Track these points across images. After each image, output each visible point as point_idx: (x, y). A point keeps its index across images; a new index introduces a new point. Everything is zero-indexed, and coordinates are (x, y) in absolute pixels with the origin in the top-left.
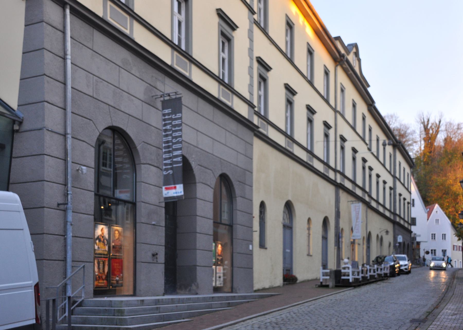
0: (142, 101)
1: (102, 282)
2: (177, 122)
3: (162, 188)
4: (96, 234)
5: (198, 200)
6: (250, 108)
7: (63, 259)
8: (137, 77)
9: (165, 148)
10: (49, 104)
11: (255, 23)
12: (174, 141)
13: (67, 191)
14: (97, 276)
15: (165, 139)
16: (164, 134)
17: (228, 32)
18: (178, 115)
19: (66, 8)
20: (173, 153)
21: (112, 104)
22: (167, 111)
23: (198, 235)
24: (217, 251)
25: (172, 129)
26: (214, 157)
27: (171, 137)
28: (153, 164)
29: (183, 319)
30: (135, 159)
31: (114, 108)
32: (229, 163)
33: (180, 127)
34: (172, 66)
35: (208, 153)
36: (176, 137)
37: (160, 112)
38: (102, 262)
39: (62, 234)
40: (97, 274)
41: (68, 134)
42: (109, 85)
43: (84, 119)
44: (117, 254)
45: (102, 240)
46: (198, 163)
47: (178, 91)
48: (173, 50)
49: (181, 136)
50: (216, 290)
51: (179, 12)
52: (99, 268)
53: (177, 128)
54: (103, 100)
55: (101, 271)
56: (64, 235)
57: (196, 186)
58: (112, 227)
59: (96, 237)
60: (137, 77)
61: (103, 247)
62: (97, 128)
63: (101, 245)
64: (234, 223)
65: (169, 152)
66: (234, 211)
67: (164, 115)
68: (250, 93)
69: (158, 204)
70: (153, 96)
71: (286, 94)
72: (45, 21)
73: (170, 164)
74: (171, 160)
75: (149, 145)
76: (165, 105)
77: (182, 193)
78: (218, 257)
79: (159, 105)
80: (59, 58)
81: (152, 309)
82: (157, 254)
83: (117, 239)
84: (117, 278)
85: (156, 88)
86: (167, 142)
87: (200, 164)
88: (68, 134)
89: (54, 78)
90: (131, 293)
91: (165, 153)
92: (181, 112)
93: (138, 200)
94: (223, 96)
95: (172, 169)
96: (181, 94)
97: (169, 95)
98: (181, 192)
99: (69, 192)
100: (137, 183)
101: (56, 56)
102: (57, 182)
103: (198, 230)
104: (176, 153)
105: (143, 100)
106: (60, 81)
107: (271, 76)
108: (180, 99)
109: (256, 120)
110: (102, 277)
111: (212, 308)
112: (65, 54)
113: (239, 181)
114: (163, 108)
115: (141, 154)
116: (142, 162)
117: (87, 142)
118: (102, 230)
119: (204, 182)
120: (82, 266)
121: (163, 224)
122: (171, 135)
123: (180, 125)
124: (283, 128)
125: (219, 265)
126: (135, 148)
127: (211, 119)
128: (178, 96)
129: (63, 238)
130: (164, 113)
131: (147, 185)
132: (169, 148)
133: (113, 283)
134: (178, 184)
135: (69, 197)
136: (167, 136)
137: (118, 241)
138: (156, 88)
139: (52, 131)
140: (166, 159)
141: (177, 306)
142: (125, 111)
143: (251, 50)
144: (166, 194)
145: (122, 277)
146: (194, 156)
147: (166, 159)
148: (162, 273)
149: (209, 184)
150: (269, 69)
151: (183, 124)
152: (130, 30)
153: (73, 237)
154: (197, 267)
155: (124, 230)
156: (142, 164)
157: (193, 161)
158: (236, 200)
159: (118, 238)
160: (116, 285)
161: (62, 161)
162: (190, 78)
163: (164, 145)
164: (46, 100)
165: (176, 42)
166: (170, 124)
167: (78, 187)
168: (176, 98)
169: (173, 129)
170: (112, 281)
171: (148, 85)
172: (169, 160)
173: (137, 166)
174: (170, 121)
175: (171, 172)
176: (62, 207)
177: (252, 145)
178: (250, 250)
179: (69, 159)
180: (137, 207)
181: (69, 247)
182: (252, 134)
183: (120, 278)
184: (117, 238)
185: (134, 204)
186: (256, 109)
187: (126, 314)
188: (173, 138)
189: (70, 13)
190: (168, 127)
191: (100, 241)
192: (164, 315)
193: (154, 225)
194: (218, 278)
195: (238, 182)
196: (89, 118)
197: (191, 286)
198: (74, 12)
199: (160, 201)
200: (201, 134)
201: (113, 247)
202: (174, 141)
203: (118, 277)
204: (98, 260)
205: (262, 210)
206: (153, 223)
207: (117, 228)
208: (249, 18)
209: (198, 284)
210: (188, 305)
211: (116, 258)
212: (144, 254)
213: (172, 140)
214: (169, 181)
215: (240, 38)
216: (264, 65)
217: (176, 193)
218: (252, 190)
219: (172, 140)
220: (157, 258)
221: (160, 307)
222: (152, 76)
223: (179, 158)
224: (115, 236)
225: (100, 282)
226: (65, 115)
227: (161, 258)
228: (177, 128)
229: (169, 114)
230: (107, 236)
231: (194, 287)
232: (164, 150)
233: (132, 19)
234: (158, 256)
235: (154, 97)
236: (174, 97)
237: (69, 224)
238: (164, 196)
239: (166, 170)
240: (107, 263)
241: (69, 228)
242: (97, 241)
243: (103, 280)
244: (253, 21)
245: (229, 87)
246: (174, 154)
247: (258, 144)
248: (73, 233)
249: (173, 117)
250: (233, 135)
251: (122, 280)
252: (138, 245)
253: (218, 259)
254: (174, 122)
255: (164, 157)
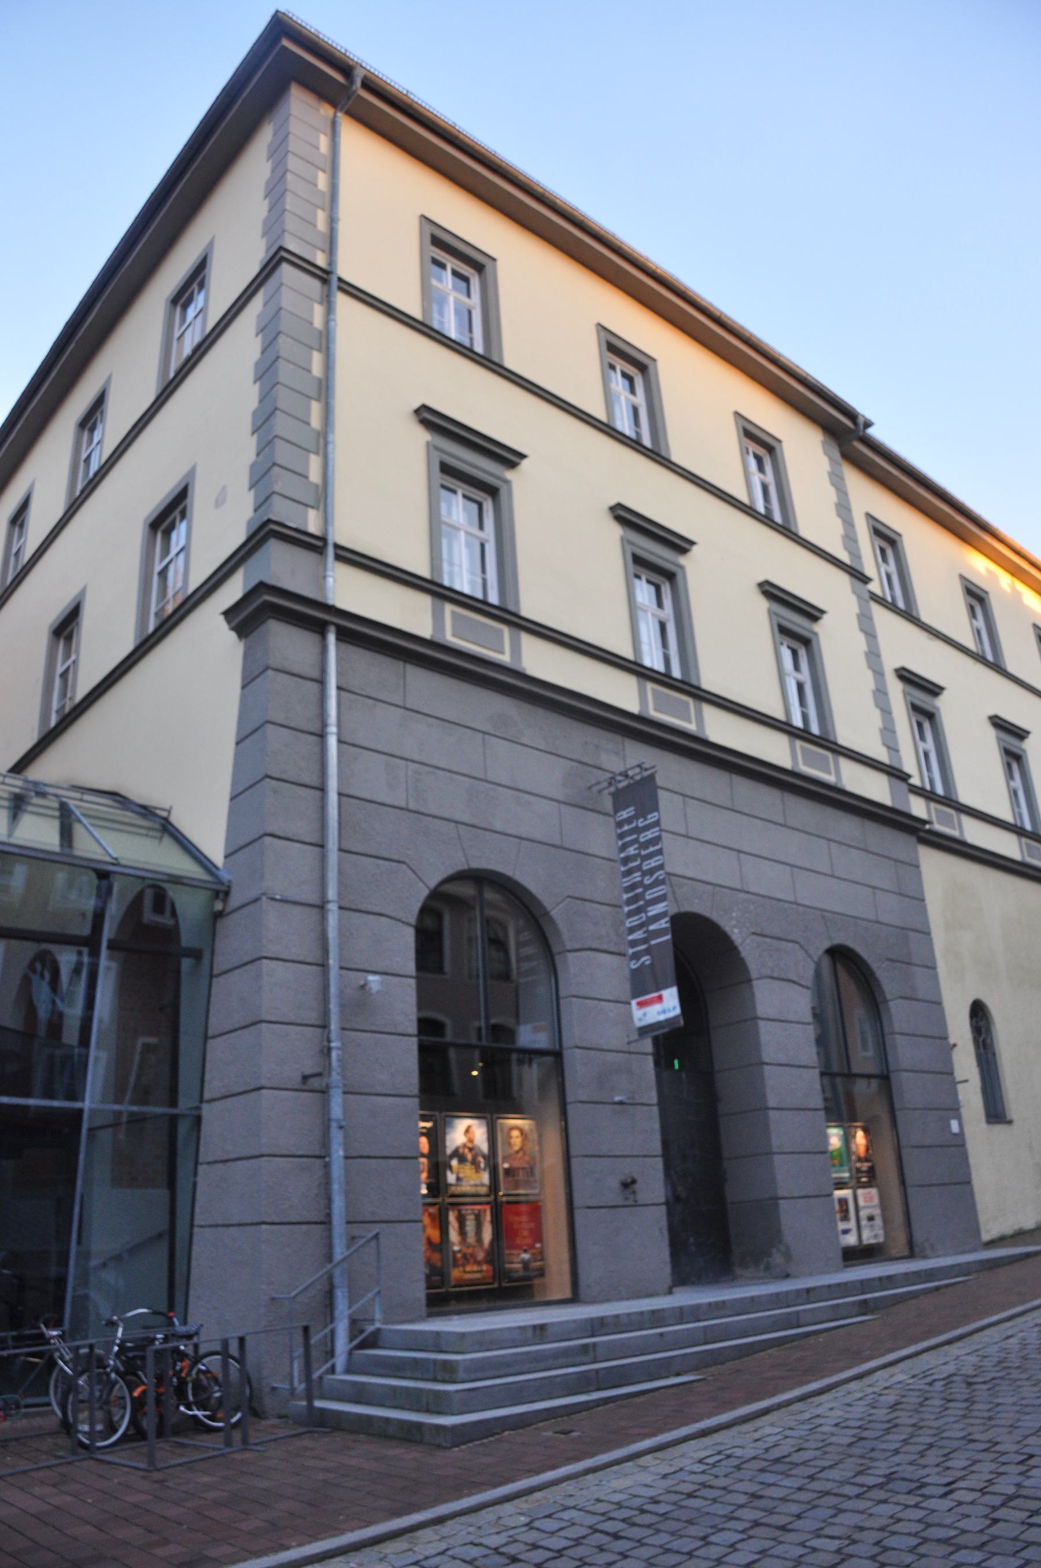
0: (558, 801)
1: (475, 1268)
2: (650, 834)
3: (629, 1003)
4: (448, 1143)
5: (761, 1023)
6: (897, 783)
7: (323, 1219)
8: (541, 750)
9: (629, 902)
10: (275, 840)
11: (872, 598)
12: (647, 881)
13: (329, 1041)
14: (459, 1255)
15: (627, 882)
16: (623, 869)
17: (795, 624)
18: (649, 817)
19: (328, 632)
20: (646, 912)
21: (466, 819)
22: (624, 815)
23: (773, 1115)
24: (853, 1147)
25: (638, 853)
26: (801, 908)
27: (639, 874)
28: (605, 947)
29: (678, 1374)
30: (551, 942)
31: (473, 826)
32: (851, 917)
33: (657, 844)
34: (645, 715)
35: (779, 900)
36: (651, 872)
37: (611, 820)
38: (472, 1217)
39: (317, 1153)
40: (456, 1248)
41: (328, 902)
42: (454, 776)
43: (381, 862)
44: (522, 1192)
45: (469, 1157)
46: (753, 930)
47: (644, 760)
48: (642, 681)
49: (661, 867)
50: (855, 1255)
51: (797, 667)
52: (462, 1232)
53: (651, 849)
54: (436, 813)
55: (471, 1238)
56: (323, 1156)
57: (751, 987)
58: (500, 1121)
59: (449, 1151)
60: (541, 750)
61: (475, 1176)
62: (421, 880)
63: (467, 1171)
64: (891, 1068)
65: (639, 911)
66: (887, 1038)
67: (620, 824)
68: (889, 748)
69: (626, 1049)
70: (590, 788)
71: (999, 739)
72: (273, 665)
73: (645, 941)
74: (645, 929)
75: (587, 904)
76: (621, 799)
77: (678, 1011)
78: (858, 1165)
79: (608, 804)
80: (308, 736)
81: (566, 1352)
82: (634, 1182)
83: (517, 1152)
84: (526, 1256)
85: (600, 768)
86: (633, 887)
87: (759, 931)
88: (328, 902)
89: (291, 779)
90: (567, 1294)
91: (630, 914)
92: (656, 809)
93: (566, 1043)
94: (805, 763)
95: (647, 952)
96: (654, 767)
97: (627, 776)
98: (674, 1008)
99: (333, 1045)
100: (562, 1002)
101: (299, 734)
102: (299, 1021)
103: (772, 1103)
104: (654, 910)
105: (561, 798)
106: (312, 784)
107: (943, 705)
108: (652, 778)
109: (918, 808)
110: (473, 1255)
111: (799, 1326)
112: (324, 725)
113: (889, 959)
114: (617, 809)
115: (561, 925)
116: (568, 948)
117: (393, 914)
118: (467, 1131)
119: (775, 975)
120: (370, 1235)
121: (653, 1097)
122: (639, 868)
123: (657, 840)
124: (1007, 816)
125: (864, 1186)
126: (546, 913)
127: (782, 821)
128: (646, 774)
129: (318, 1162)
130: (618, 819)
131: (587, 1001)
132: (638, 902)
133: (511, 1271)
134: (666, 987)
135: (334, 1055)
136: (629, 873)
137: (520, 1154)
138: (600, 768)
139: (284, 901)
140: (632, 930)
141: (661, 1335)
142: (508, 831)
143: (873, 656)
144: (640, 1020)
145: (541, 1252)
146: (734, 915)
147: (632, 930)
148: (660, 1229)
149: (795, 979)
150: (936, 690)
151: (664, 834)
152: (697, 723)
153: (346, 1158)
154: (780, 1202)
155: (540, 1127)
156: (569, 951)
157: (735, 926)
158: (888, 1009)
159: (521, 1149)
160: (521, 1273)
161: (314, 968)
162: (701, 735)
163: (625, 896)
164: (269, 831)
165: (798, 722)
166: (636, 841)
167: (366, 1028)
168: (642, 779)
169: (643, 853)
170: (507, 1266)
171: (576, 764)
172: (641, 932)
173: (557, 958)
174: (635, 836)
175: (646, 959)
176: (315, 1083)
177: (918, 867)
178: (955, 1134)
179: (331, 962)
180: (565, 1061)
181: (335, 1187)
182: (914, 840)
183: (533, 1254)
184: (516, 1148)
185: (557, 1055)
186: (912, 781)
187: (461, 1375)
188: (645, 874)
189: (338, 639)
190: (631, 851)
191: (462, 1159)
192: (597, 1371)
193: (621, 1103)
194: (864, 1222)
195: (887, 963)
196: (396, 857)
197: (770, 1255)
198: (345, 636)
199: (631, 1039)
200: (723, 856)
201: (507, 1172)
202: (647, 881)
203: (525, 1251)
204: (459, 1211)
205: (982, 1024)
206: (617, 1099)
207: (516, 1125)
208: (854, 592)
209: (788, 1248)
210: (705, 1327)
211: (518, 1203)
212: (597, 1183)
213: (642, 882)
214: (643, 985)
215: (838, 636)
216: (920, 687)
217: (664, 1012)
218: (935, 978)
219: (642, 882)
220: (634, 1192)
221: (595, 1344)
222: (586, 743)
223: (663, 921)
224: (510, 1144)
225: (468, 1269)
226: (323, 859)
227: (654, 1186)
228: (651, 849)
229: (629, 821)
230: (485, 1147)
231: (777, 1259)
232: (626, 909)
233: (515, 631)
234: (636, 1187)
235: (595, 789)
236: (638, 778)
237: (334, 1125)
238: (638, 1024)
239: (636, 956)
240: (488, 1217)
241: (337, 1138)
242: (454, 1163)
243: (479, 1263)
244: (867, 596)
245: (827, 743)
246: (650, 914)
247: (933, 864)
248: (345, 1150)
249: (641, 823)
250: (853, 850)
251: (542, 1260)
252: (574, 1162)
253: (858, 1170)
254: (643, 835)
255: (628, 925)
